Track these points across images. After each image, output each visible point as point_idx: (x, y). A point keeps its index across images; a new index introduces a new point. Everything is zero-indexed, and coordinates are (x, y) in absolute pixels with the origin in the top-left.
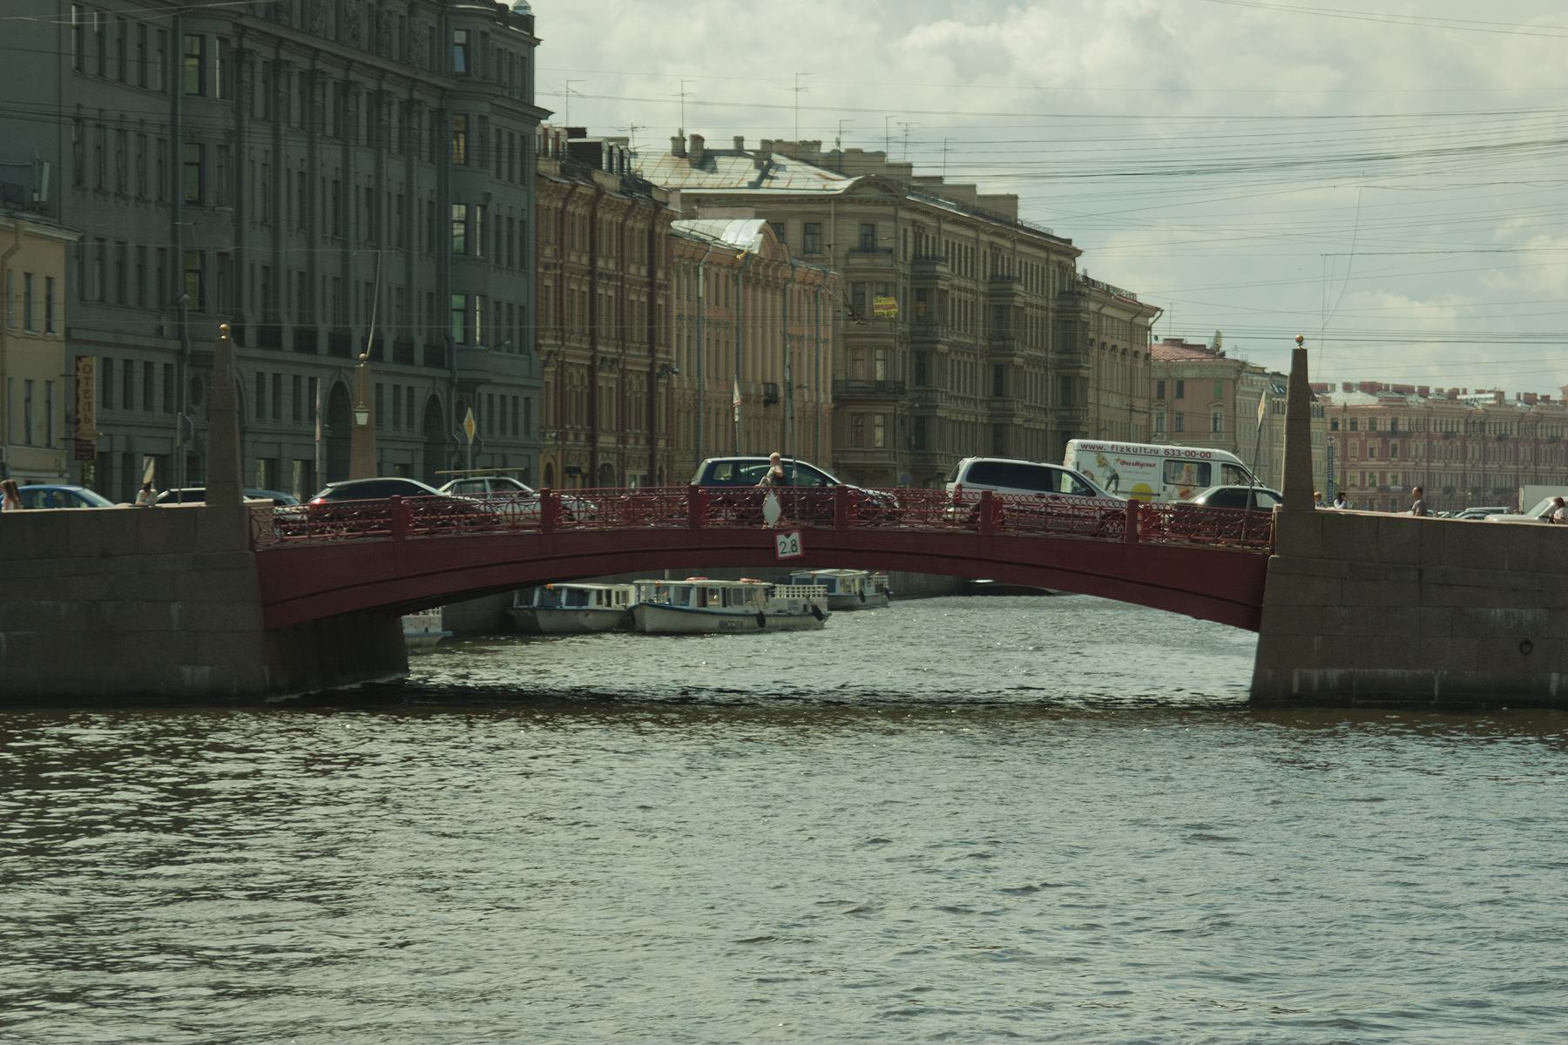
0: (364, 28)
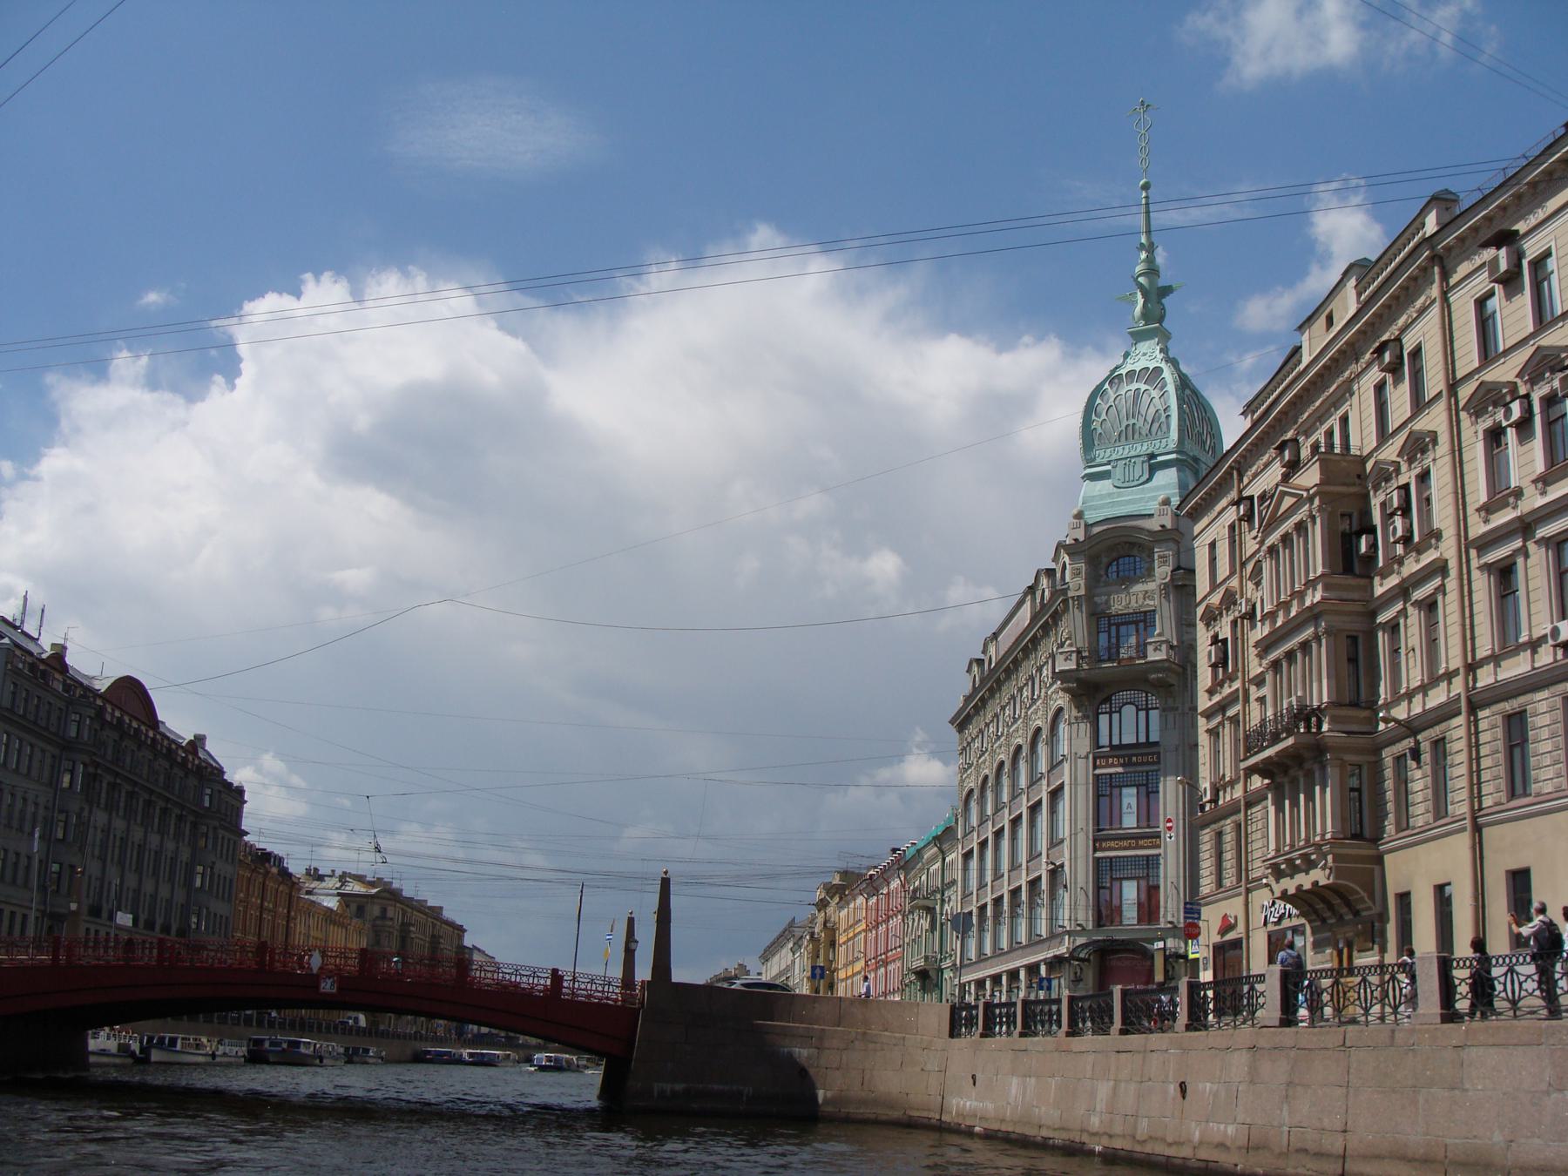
0: (161, 779)
